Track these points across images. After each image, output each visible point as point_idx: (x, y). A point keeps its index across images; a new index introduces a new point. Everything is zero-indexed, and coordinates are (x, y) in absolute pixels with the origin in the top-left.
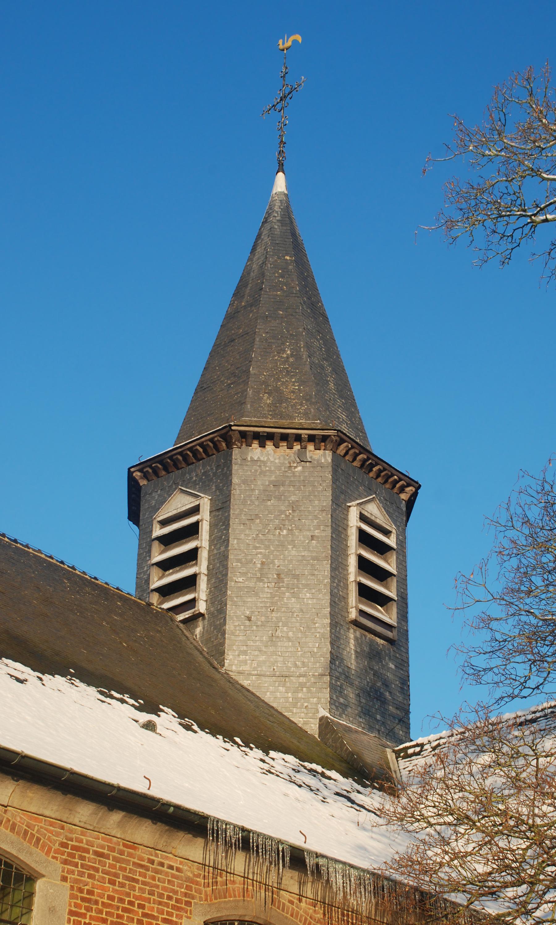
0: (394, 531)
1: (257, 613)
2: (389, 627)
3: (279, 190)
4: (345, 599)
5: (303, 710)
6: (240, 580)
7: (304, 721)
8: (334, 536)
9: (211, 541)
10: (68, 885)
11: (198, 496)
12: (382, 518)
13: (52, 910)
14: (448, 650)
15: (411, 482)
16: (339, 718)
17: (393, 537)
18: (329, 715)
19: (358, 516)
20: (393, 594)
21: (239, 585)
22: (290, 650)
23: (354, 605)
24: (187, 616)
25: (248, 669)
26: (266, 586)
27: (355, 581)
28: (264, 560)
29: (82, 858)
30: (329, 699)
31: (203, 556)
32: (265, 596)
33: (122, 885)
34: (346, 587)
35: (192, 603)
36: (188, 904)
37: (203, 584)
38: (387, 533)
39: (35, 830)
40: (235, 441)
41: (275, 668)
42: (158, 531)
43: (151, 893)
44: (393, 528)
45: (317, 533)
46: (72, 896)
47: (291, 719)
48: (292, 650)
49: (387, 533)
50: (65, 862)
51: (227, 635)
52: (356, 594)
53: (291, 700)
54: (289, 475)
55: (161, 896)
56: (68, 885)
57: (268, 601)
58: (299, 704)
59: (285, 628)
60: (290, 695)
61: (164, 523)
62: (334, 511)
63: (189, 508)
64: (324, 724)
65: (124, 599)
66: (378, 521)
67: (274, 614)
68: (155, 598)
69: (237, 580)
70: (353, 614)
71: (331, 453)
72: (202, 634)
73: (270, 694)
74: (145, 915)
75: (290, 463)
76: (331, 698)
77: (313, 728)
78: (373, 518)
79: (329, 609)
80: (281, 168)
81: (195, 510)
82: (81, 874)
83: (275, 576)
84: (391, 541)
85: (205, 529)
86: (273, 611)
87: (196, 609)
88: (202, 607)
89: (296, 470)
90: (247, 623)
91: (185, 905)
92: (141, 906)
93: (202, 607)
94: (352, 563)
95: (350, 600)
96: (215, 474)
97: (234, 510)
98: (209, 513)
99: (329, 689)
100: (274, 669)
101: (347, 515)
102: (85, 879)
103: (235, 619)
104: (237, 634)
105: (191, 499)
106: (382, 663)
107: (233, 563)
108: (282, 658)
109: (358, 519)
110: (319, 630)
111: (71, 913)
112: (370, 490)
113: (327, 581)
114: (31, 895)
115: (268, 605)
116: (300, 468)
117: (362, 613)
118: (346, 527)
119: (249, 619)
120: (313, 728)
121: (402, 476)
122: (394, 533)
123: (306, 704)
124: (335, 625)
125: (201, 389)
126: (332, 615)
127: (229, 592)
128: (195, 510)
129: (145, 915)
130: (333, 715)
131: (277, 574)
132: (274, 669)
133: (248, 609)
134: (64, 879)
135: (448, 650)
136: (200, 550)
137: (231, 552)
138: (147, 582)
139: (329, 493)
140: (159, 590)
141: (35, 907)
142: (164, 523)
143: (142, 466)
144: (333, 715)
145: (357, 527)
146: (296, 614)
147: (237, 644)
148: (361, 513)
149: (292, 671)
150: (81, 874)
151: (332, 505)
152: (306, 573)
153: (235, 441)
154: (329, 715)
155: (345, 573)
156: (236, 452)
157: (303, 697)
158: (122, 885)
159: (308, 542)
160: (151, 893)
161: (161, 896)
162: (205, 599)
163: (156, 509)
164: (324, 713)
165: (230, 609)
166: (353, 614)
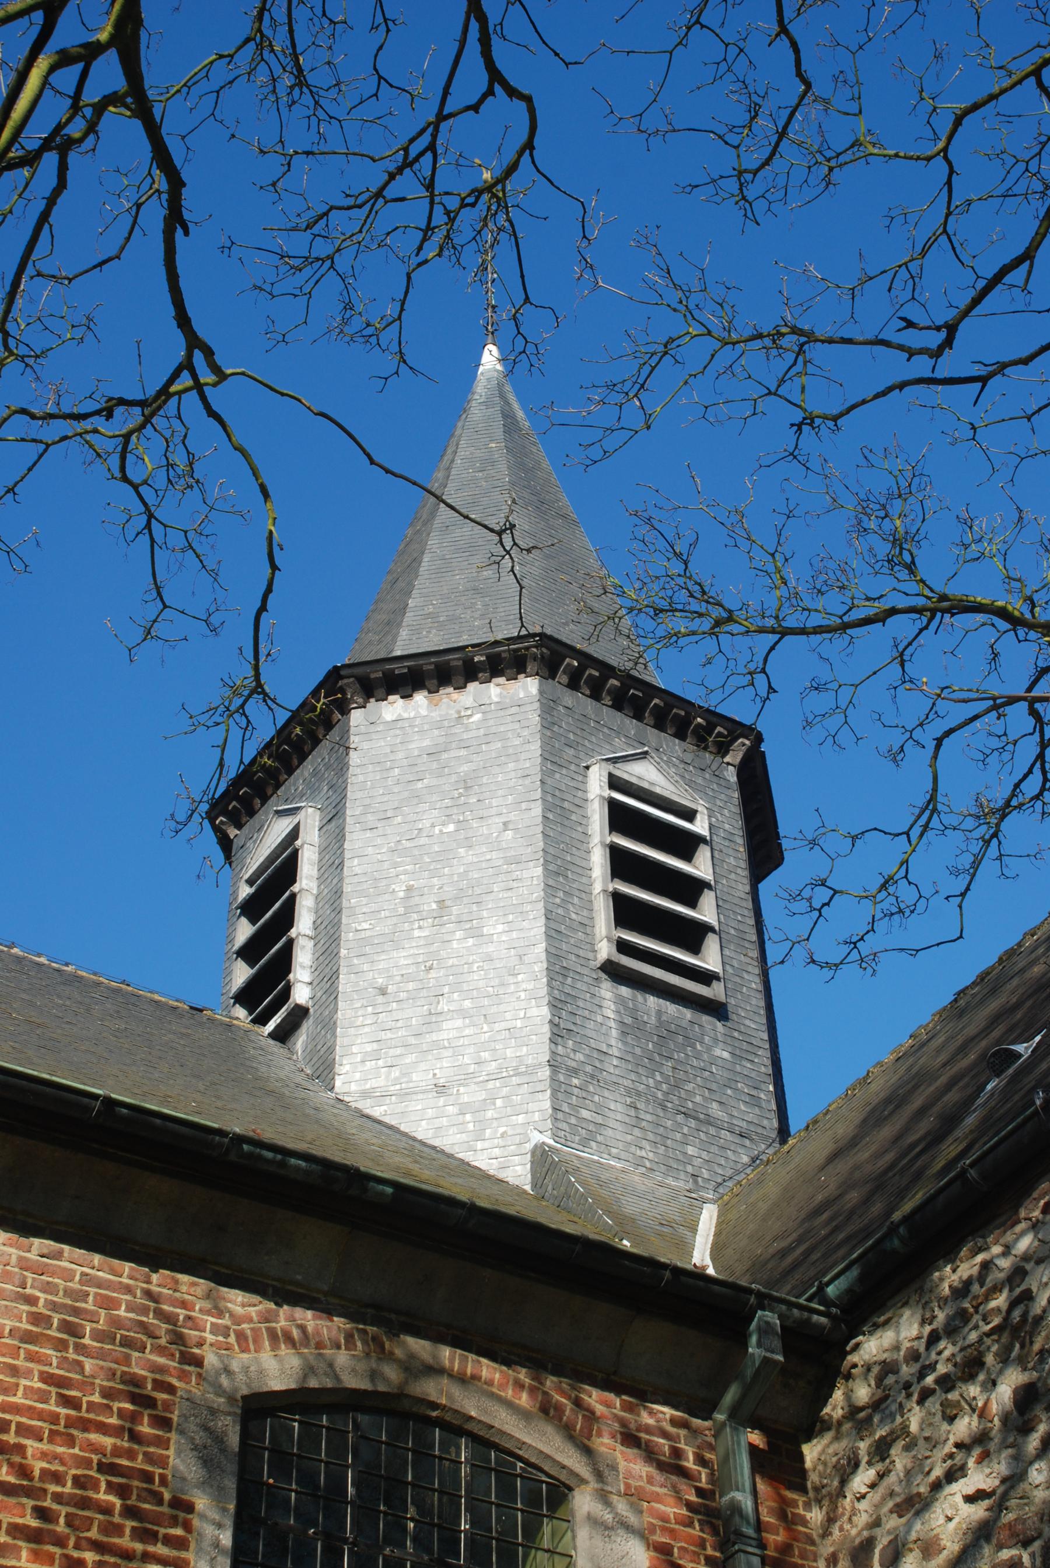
0: (700, 809)
1: (398, 978)
2: (706, 977)
3: (488, 367)
5: (496, 1141)
6: (365, 926)
7: (500, 1163)
8: (550, 816)
11: (298, 808)
12: (672, 788)
16: (581, 1148)
18: (551, 1142)
19: (606, 780)
21: (363, 935)
22: (467, 1032)
23: (604, 933)
24: (279, 1021)
25: (382, 1084)
26: (416, 925)
27: (605, 891)
28: (412, 883)
30: (550, 1111)
32: (414, 944)
34: (588, 906)
40: (352, 697)
41: (437, 1071)
45: (512, 817)
47: (473, 1163)
48: (472, 1032)
49: (690, 815)
51: (338, 1030)
52: (607, 920)
53: (471, 1126)
54: (457, 731)
57: (421, 951)
58: (488, 1131)
59: (456, 995)
60: (468, 1117)
63: (287, 836)
66: (658, 790)
67: (433, 974)
69: (359, 928)
70: (605, 951)
71: (537, 681)
73: (428, 1124)
75: (459, 712)
76: (555, 1109)
78: (646, 785)
79: (544, 945)
80: (492, 333)
83: (434, 906)
86: (431, 968)
87: (291, 1000)
89: (471, 720)
90: (380, 999)
91: (91, 1461)
94: (598, 862)
95: (597, 930)
97: (352, 811)
98: (317, 832)
99: (549, 1092)
100: (435, 1075)
101: (584, 783)
103: (356, 997)
104: (359, 1023)
106: (694, 1048)
107: (351, 900)
108: (451, 1050)
109: (606, 787)
110: (524, 986)
113: (539, 893)
115: (420, 960)
116: (477, 717)
119: (383, 992)
122: (703, 813)
123: (502, 1130)
127: (343, 952)
130: (563, 1141)
131: (439, 902)
132: (435, 1075)
133: (380, 974)
136: (298, 897)
137: (347, 881)
139: (535, 748)
144: (563, 1141)
145: (602, 797)
146: (476, 965)
147: (359, 1041)
148: (611, 775)
149: (471, 1071)
151: (542, 765)
152: (496, 889)
153: (352, 697)
154: (551, 1142)
155: (584, 880)
157: (495, 1116)
159: (498, 836)
162: (308, 979)
164: (537, 1138)
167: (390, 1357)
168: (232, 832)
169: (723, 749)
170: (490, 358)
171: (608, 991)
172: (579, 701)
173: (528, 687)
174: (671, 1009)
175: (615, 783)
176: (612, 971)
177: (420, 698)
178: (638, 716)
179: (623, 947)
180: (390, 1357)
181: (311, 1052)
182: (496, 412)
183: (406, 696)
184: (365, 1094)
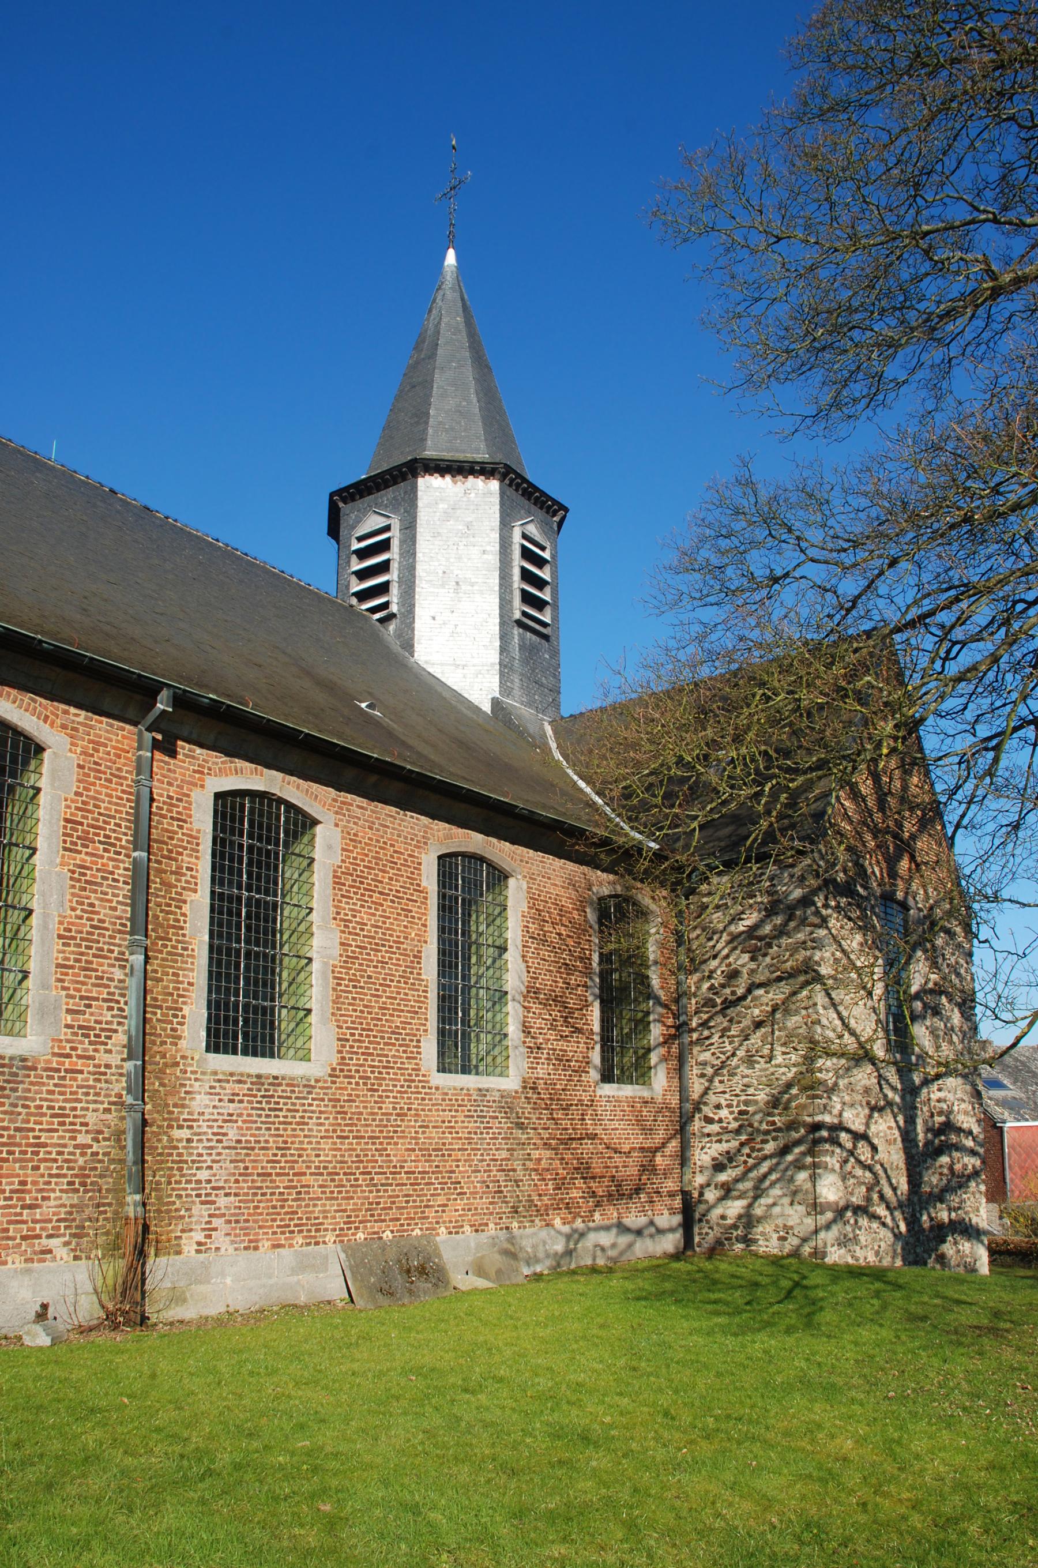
2: (544, 625)
4: (511, 602)
9: (401, 555)
10: (339, 829)
13: (330, 847)
14: (1025, 905)
15: (566, 510)
17: (548, 551)
20: (548, 598)
29: (348, 810)
31: (394, 566)
33: (378, 830)
34: (511, 592)
35: (385, 606)
36: (426, 843)
37: (394, 590)
38: (543, 549)
39: (723, 787)
42: (356, 546)
43: (399, 836)
44: (547, 544)
46: (343, 838)
49: (543, 549)
50: (337, 813)
55: (406, 838)
56: (339, 829)
61: (360, 539)
62: (501, 530)
64: (495, 703)
65: (318, 598)
68: (354, 601)
70: (517, 615)
72: (395, 631)
74: (395, 852)
77: (487, 707)
80: (451, 241)
81: (387, 529)
82: (348, 822)
84: (546, 555)
85: (395, 544)
88: (394, 608)
92: (392, 845)
93: (394, 608)
96: (403, 499)
102: (351, 825)
105: (383, 519)
111: (343, 850)
112: (529, 513)
113: (497, 588)
114: (314, 836)
117: (524, 614)
118: (511, 544)
120: (487, 707)
121: (555, 502)
124: (502, 624)
125: (387, 427)
126: (501, 616)
128: (387, 529)
129: (395, 852)
134: (337, 825)
135: (1025, 905)
138: (348, 587)
140: (356, 594)
141: (317, 845)
142: (360, 539)
143: (339, 492)
150: (348, 822)
156: (420, 481)
158: (378, 830)
160: (399, 836)
161: (406, 838)
163: (353, 527)
165: (418, 611)
166: (517, 615)
167: (836, 1084)
168: (341, 505)
169: (554, 515)
170: (451, 258)
171: (517, 631)
172: (517, 497)
173: (494, 485)
174: (534, 637)
175: (525, 536)
176: (519, 623)
177: (448, 478)
178: (529, 499)
179: (524, 614)
180: (836, 1084)
181: (399, 635)
182: (457, 295)
183: (443, 476)
184: (426, 662)
